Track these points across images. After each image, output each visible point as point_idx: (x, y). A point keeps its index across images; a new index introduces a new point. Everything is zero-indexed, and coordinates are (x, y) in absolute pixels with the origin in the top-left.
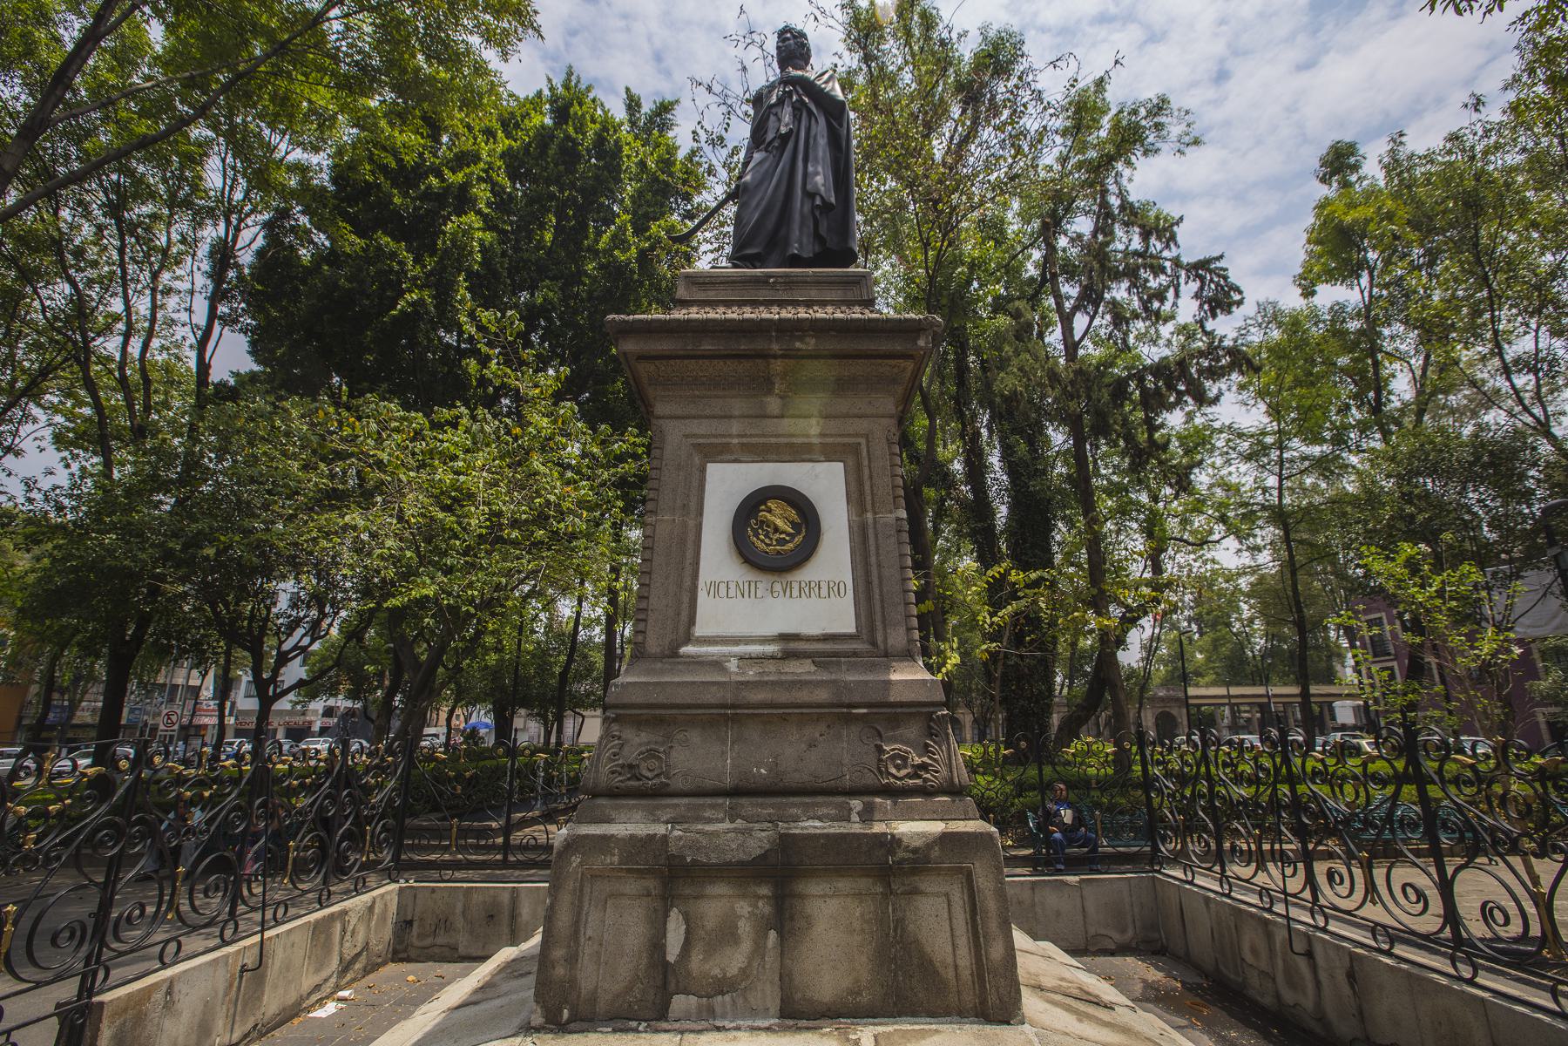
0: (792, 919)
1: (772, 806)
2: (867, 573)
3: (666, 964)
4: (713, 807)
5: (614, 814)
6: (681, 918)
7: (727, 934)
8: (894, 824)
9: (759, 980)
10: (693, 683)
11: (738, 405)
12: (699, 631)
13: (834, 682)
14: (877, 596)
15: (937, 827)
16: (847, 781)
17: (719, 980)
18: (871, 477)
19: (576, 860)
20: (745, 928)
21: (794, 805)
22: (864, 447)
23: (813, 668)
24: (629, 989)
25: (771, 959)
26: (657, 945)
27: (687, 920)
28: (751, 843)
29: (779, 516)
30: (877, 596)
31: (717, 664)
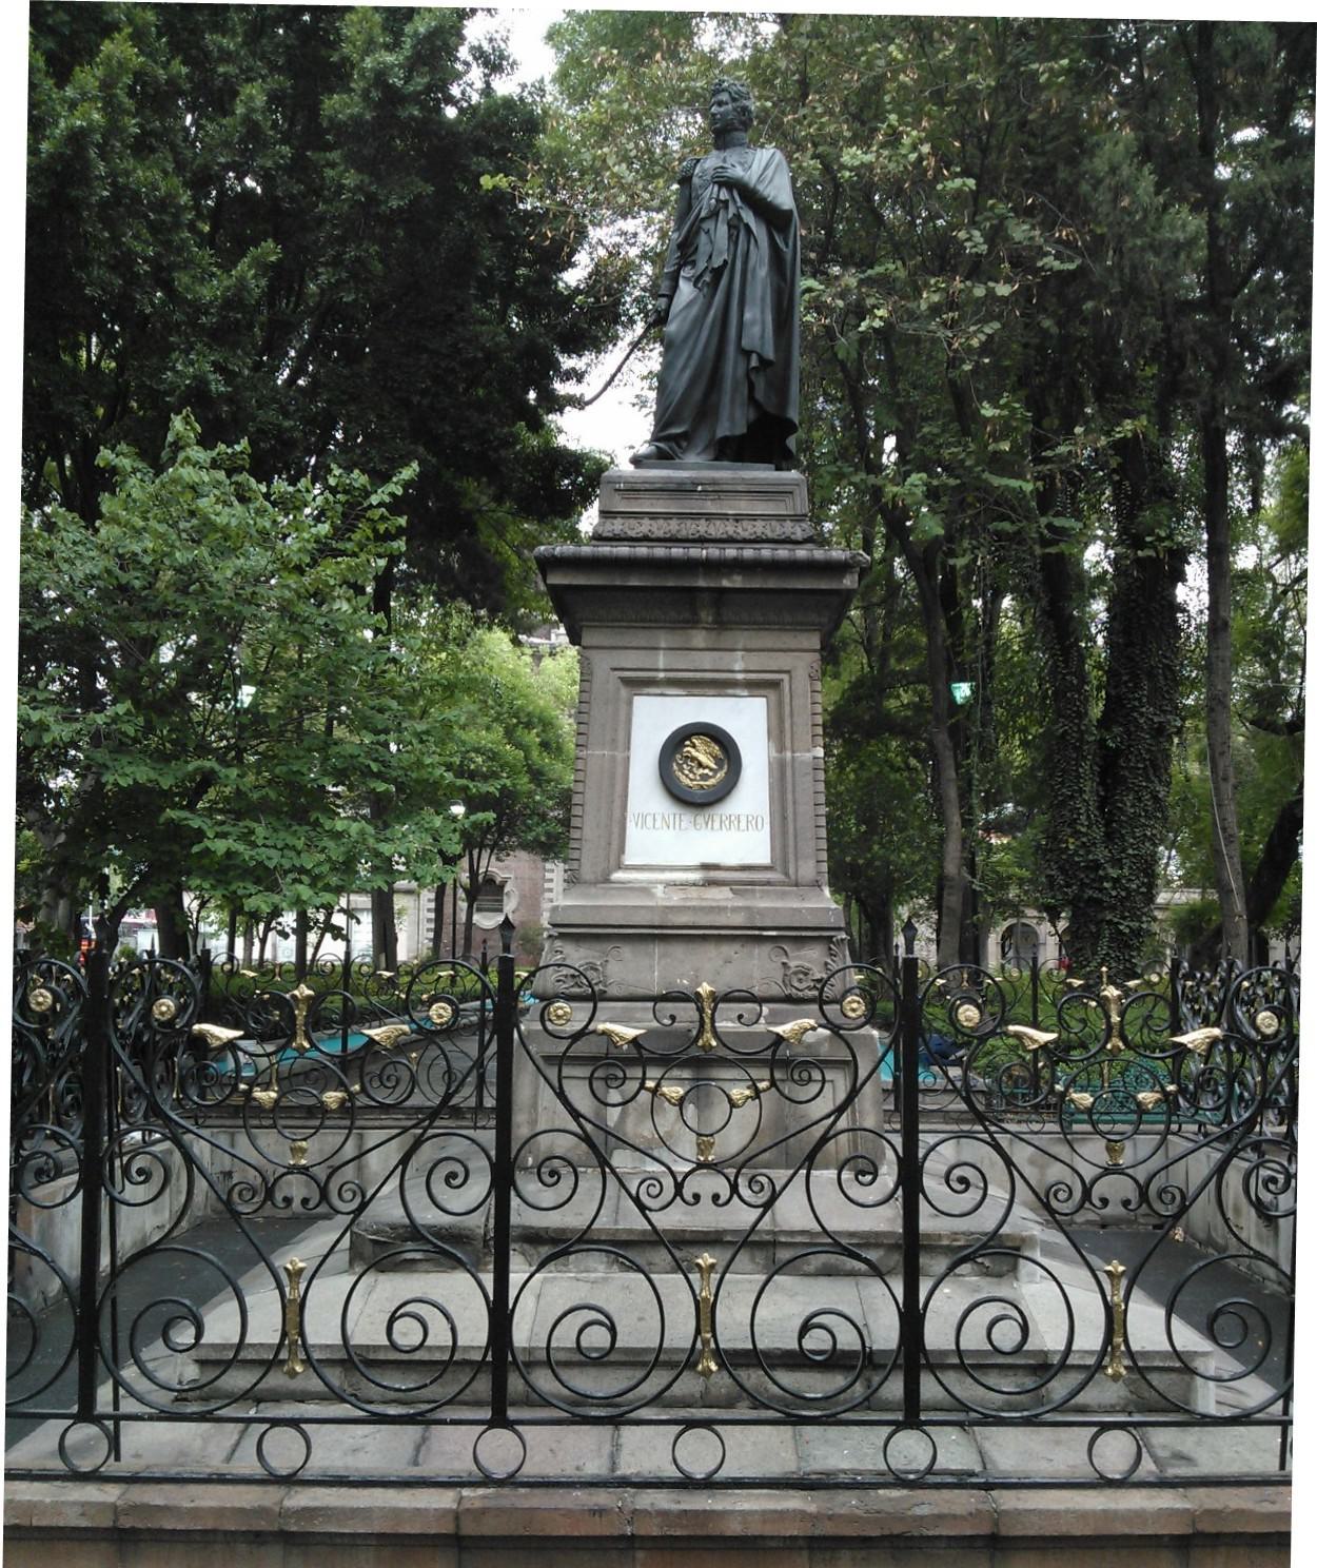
2: (784, 809)
12: (628, 860)
18: (792, 715)
29: (702, 752)
31: (645, 890)
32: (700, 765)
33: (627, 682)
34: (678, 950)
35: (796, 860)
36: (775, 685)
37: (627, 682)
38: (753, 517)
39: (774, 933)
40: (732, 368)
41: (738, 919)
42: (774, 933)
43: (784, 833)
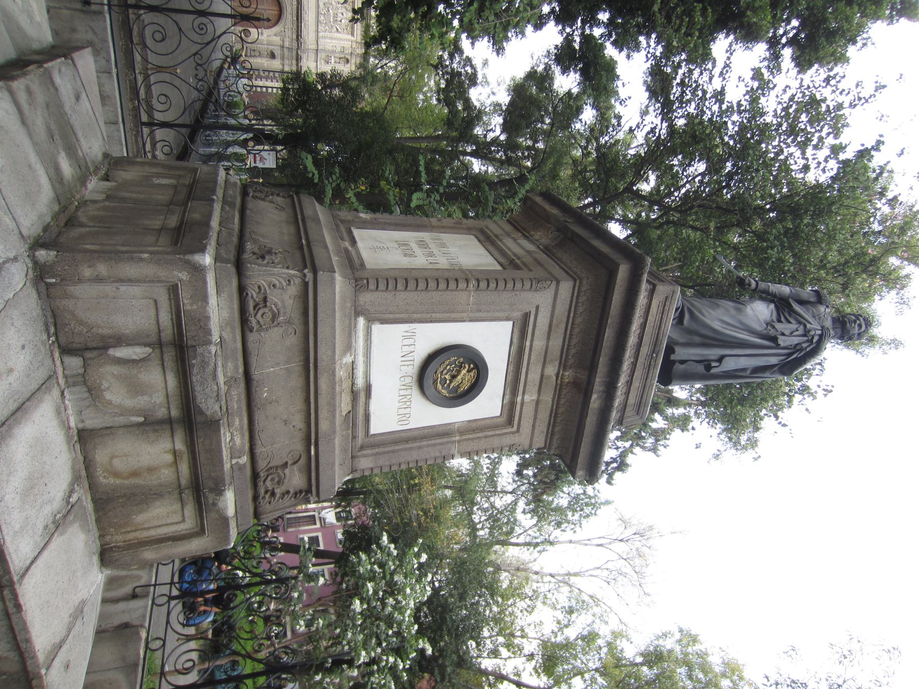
0: (155, 431)
1: (243, 444)
2: (415, 439)
3: (106, 348)
4: (236, 368)
5: (224, 295)
6: (145, 355)
7: (136, 389)
8: (232, 488)
9: (105, 414)
10: (334, 338)
11: (556, 343)
12: (376, 328)
13: (334, 432)
14: (397, 448)
15: (231, 512)
16: (259, 450)
17: (100, 387)
18: (486, 437)
19: (184, 276)
20: (142, 401)
21: (241, 420)
22: (510, 430)
23: (344, 414)
24: (81, 323)
25: (121, 420)
26: (120, 340)
27: (143, 360)
28: (211, 402)
29: (465, 377)
30: (397, 448)
31: (349, 347)
32: (454, 377)
33: (526, 316)
34: (296, 381)
35: (372, 455)
36: (510, 422)
37: (526, 316)
38: (627, 393)
39: (313, 453)
40: (713, 353)
41: (324, 426)
42: (313, 453)
43: (396, 442)
